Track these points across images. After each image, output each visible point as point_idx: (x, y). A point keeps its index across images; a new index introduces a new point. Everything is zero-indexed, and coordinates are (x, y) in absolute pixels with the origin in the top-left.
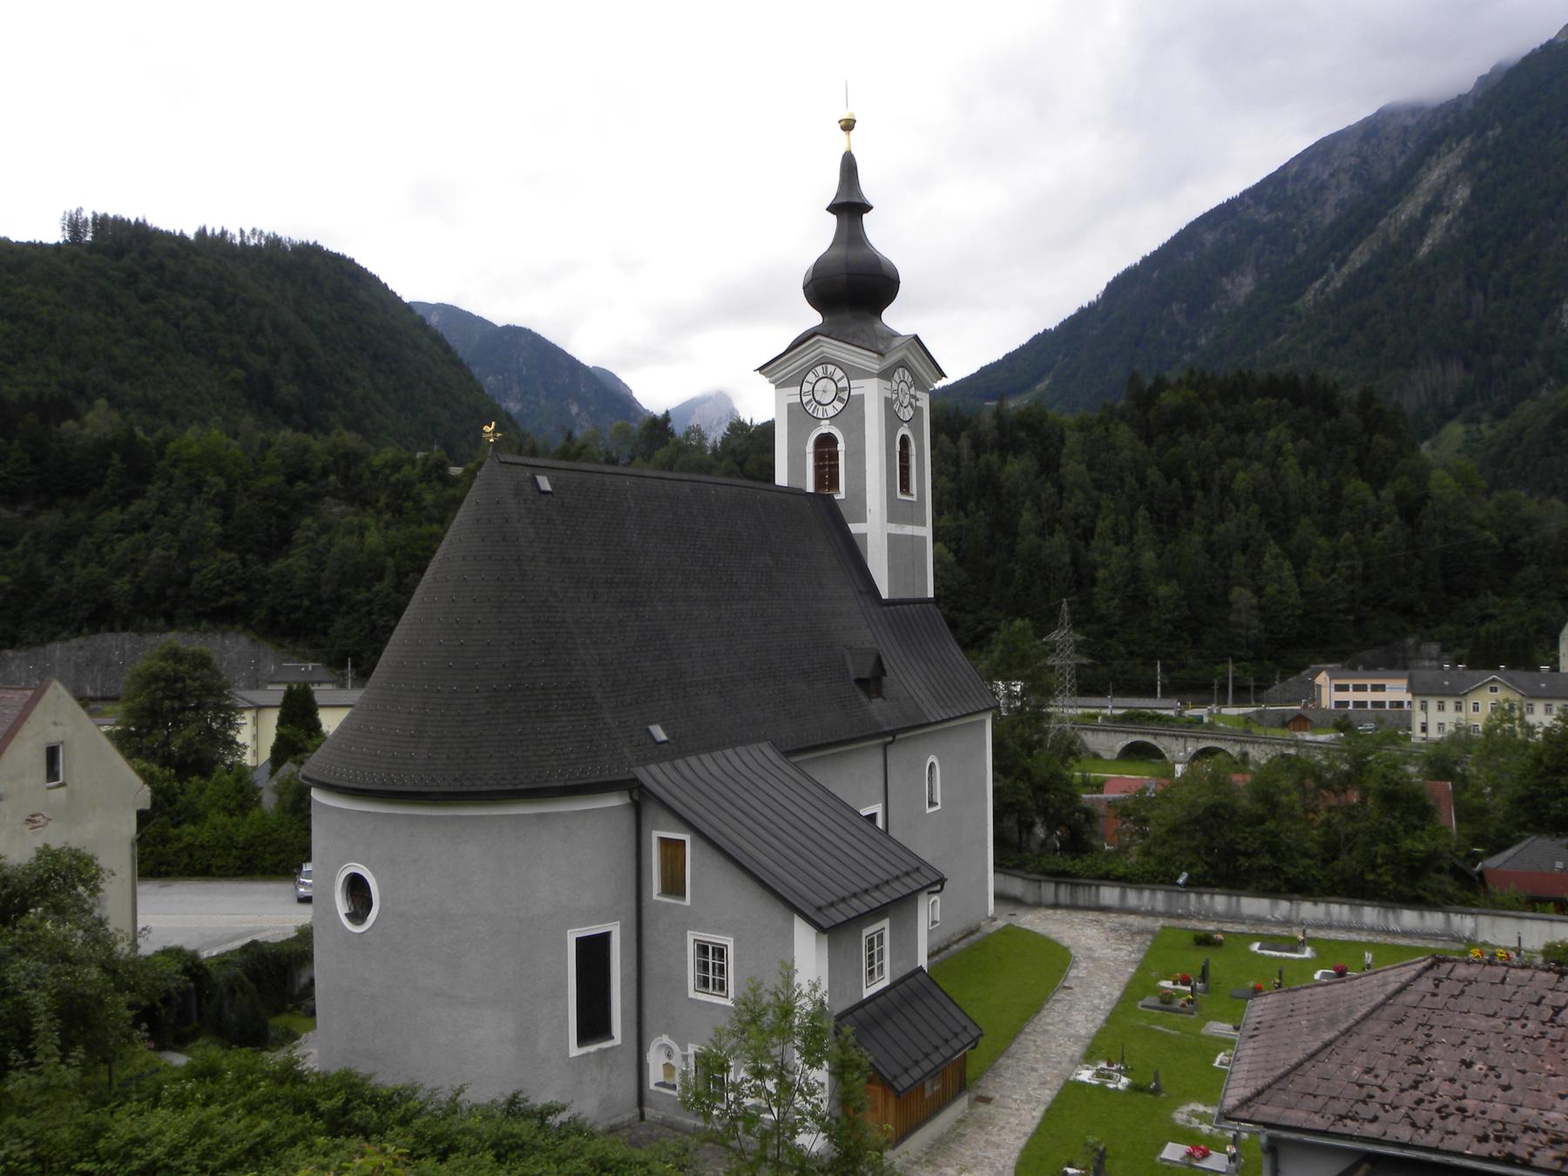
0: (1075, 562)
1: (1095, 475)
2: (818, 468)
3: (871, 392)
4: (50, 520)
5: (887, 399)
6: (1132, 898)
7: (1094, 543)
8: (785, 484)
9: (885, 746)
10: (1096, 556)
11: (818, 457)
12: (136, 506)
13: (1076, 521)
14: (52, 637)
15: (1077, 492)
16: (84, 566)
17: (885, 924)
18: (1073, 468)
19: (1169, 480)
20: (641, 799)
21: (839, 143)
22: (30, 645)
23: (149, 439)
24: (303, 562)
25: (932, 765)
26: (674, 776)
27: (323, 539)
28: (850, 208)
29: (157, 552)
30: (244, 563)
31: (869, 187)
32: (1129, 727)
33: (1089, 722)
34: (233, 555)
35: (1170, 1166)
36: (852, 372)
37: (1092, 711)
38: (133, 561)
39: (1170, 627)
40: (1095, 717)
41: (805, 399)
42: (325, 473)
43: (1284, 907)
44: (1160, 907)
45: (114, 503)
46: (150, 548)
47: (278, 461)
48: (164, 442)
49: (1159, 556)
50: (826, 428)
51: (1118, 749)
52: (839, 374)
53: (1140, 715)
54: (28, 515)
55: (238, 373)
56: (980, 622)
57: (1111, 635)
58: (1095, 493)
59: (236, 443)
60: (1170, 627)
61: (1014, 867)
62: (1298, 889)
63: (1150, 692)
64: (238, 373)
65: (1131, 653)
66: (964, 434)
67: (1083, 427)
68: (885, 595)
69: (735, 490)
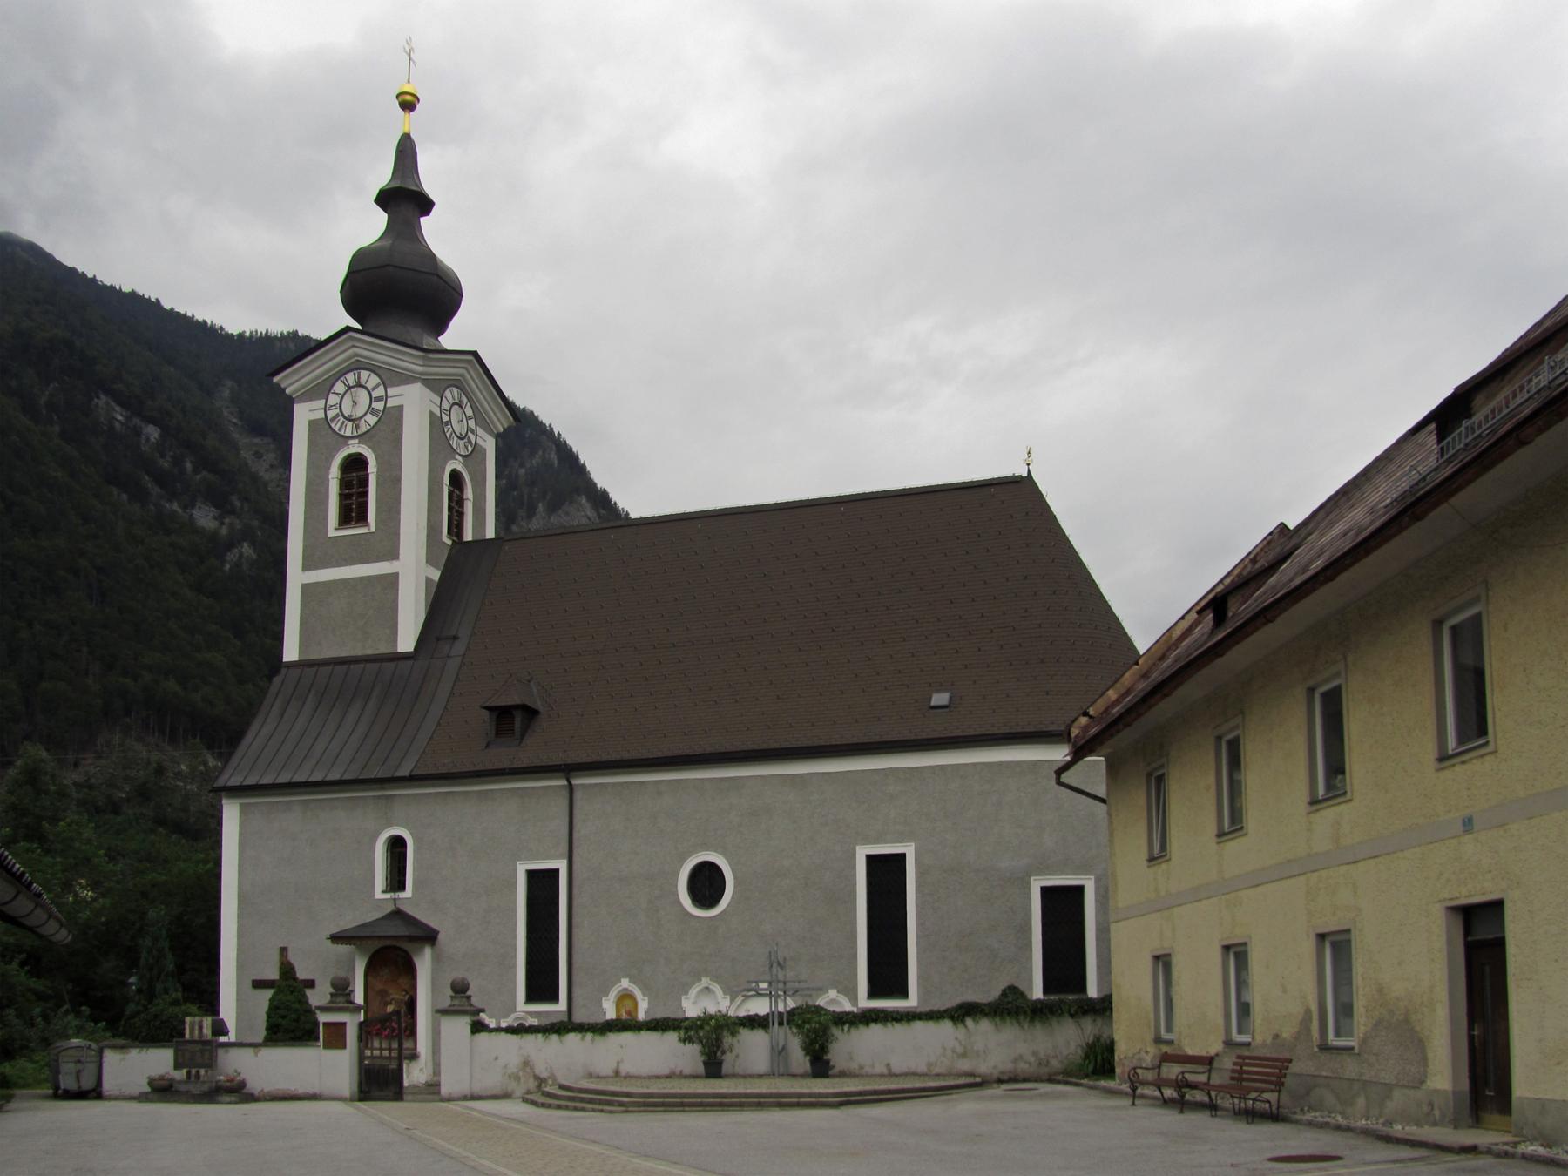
2: (344, 497)
3: (415, 403)
11: (345, 484)
21: (403, 122)
28: (405, 200)
31: (430, 179)
35: (941, 688)
36: (392, 378)
41: (330, 414)
50: (354, 448)
52: (374, 380)
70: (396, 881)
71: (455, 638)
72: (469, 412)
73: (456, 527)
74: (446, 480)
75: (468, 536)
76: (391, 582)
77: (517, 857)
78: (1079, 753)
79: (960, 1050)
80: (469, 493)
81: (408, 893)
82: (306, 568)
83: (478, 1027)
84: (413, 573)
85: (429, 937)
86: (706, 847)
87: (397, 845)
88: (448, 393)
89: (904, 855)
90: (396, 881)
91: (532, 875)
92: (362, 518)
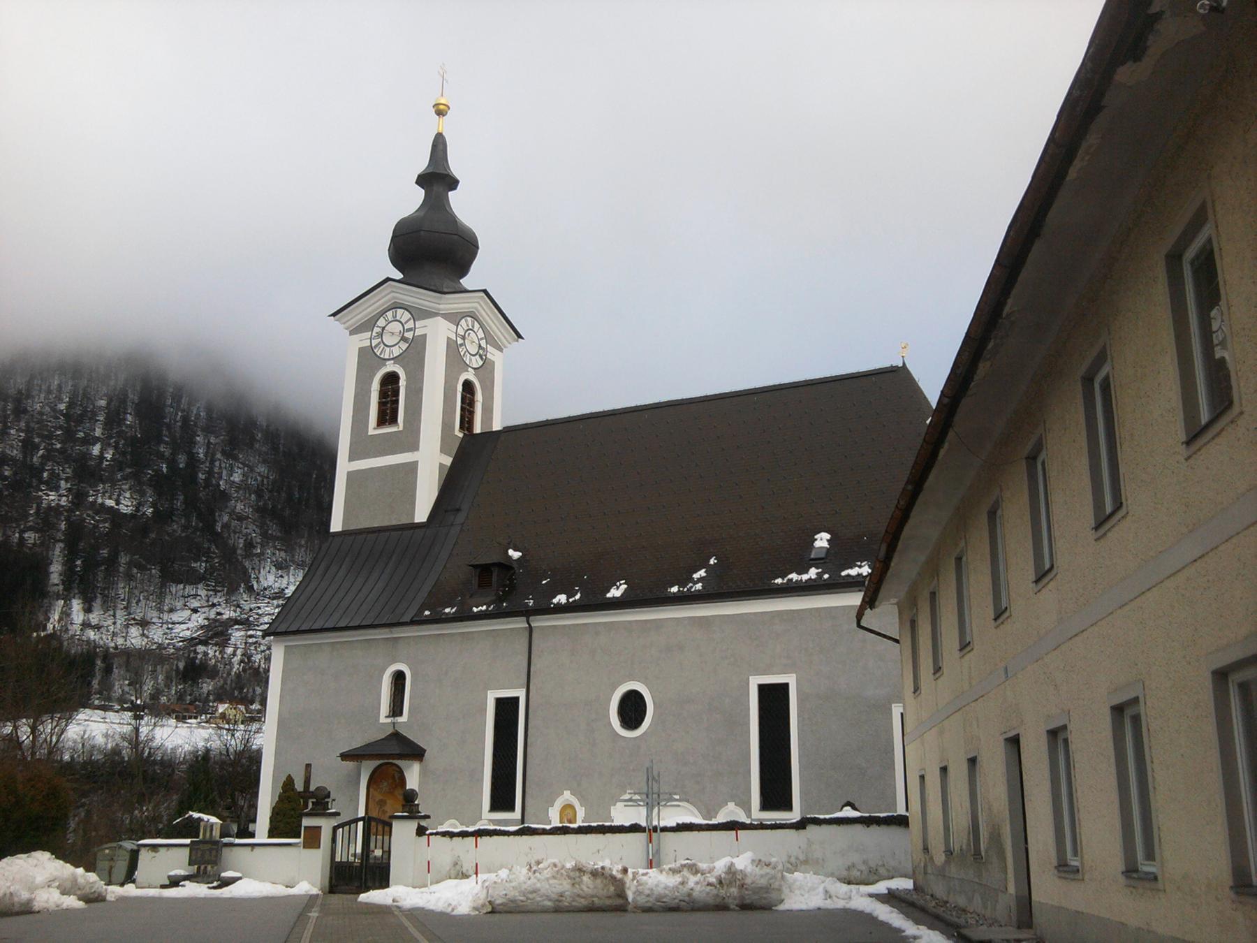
2: (382, 404)
8: (451, 459)
11: (383, 394)
21: (434, 125)
28: (437, 180)
31: (456, 166)
36: (419, 314)
50: (391, 367)
52: (407, 315)
70: (396, 709)
71: (458, 510)
72: (481, 334)
73: (467, 422)
74: (460, 388)
75: (478, 429)
76: (411, 470)
77: (487, 688)
78: (870, 602)
79: (802, 857)
80: (479, 397)
81: (404, 718)
82: (351, 459)
83: (421, 831)
84: (430, 461)
85: (417, 753)
86: (632, 678)
87: (399, 678)
88: (463, 322)
89: (786, 685)
90: (396, 709)
91: (499, 702)
92: (394, 420)
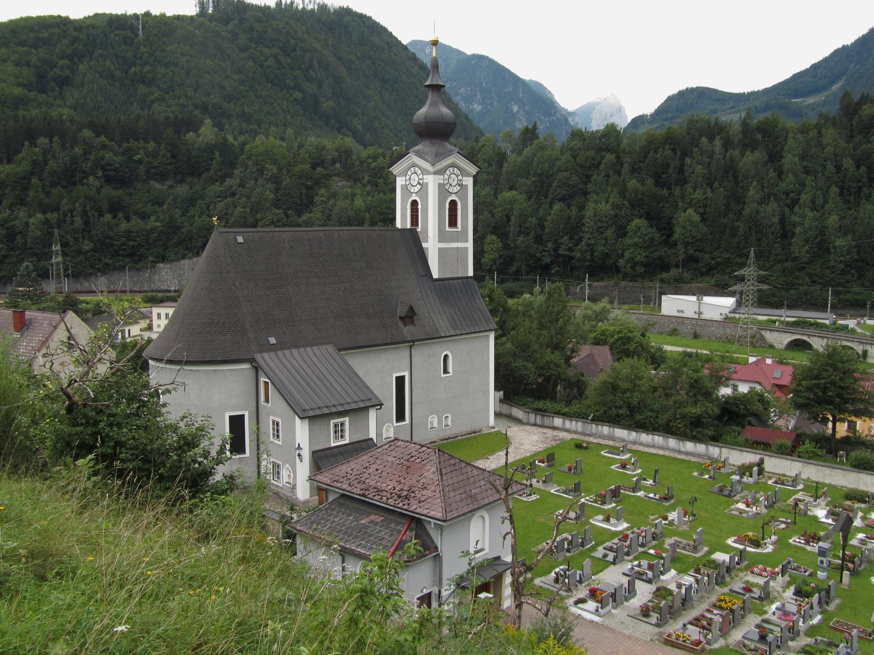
0: (782, 221)
1: (805, 163)
4: (182, 190)
5: (439, 184)
6: (568, 424)
7: (797, 209)
9: (411, 347)
10: (795, 218)
12: (228, 182)
13: (787, 194)
14: (183, 257)
15: (790, 175)
16: (200, 217)
17: (347, 419)
18: (790, 160)
19: (858, 167)
20: (257, 369)
22: (172, 261)
23: (236, 143)
24: (319, 215)
25: (446, 357)
26: (277, 361)
27: (332, 201)
29: (239, 209)
30: (287, 216)
32: (793, 329)
33: (770, 325)
34: (281, 211)
36: (425, 172)
37: (774, 318)
38: (226, 214)
39: (842, 266)
40: (774, 322)
42: (334, 162)
43: (633, 435)
44: (580, 429)
45: (217, 181)
46: (235, 206)
47: (307, 155)
48: (244, 144)
49: (842, 218)
51: (786, 342)
52: (419, 172)
53: (805, 322)
54: (170, 187)
55: (298, 95)
56: (713, 259)
57: (801, 269)
58: (803, 176)
59: (284, 144)
60: (842, 266)
61: (522, 405)
62: (640, 427)
63: (821, 307)
64: (298, 95)
65: (814, 282)
66: (718, 137)
67: (804, 130)
68: (435, 275)
69: (351, 232)
